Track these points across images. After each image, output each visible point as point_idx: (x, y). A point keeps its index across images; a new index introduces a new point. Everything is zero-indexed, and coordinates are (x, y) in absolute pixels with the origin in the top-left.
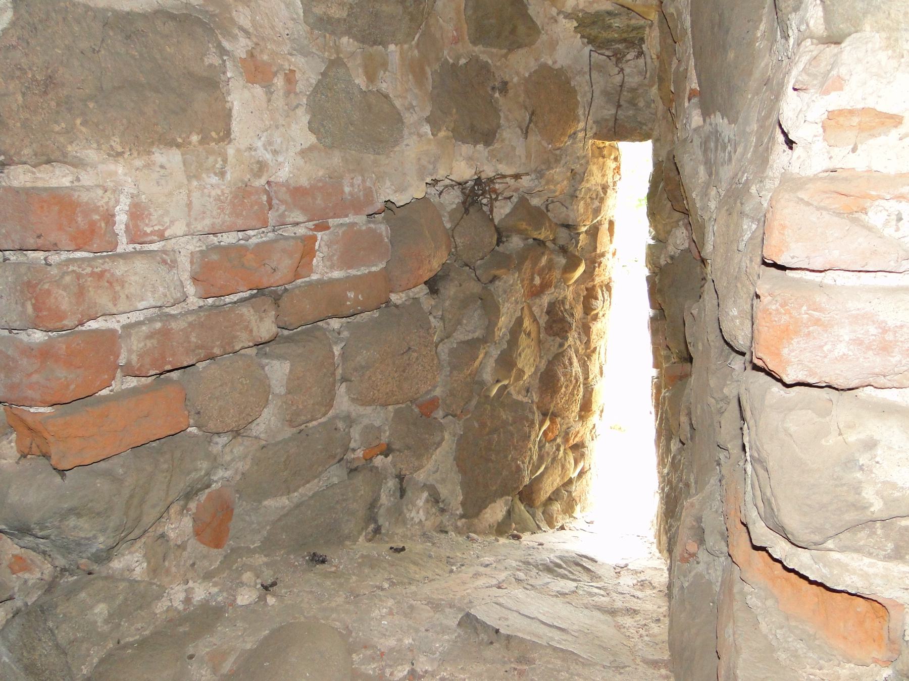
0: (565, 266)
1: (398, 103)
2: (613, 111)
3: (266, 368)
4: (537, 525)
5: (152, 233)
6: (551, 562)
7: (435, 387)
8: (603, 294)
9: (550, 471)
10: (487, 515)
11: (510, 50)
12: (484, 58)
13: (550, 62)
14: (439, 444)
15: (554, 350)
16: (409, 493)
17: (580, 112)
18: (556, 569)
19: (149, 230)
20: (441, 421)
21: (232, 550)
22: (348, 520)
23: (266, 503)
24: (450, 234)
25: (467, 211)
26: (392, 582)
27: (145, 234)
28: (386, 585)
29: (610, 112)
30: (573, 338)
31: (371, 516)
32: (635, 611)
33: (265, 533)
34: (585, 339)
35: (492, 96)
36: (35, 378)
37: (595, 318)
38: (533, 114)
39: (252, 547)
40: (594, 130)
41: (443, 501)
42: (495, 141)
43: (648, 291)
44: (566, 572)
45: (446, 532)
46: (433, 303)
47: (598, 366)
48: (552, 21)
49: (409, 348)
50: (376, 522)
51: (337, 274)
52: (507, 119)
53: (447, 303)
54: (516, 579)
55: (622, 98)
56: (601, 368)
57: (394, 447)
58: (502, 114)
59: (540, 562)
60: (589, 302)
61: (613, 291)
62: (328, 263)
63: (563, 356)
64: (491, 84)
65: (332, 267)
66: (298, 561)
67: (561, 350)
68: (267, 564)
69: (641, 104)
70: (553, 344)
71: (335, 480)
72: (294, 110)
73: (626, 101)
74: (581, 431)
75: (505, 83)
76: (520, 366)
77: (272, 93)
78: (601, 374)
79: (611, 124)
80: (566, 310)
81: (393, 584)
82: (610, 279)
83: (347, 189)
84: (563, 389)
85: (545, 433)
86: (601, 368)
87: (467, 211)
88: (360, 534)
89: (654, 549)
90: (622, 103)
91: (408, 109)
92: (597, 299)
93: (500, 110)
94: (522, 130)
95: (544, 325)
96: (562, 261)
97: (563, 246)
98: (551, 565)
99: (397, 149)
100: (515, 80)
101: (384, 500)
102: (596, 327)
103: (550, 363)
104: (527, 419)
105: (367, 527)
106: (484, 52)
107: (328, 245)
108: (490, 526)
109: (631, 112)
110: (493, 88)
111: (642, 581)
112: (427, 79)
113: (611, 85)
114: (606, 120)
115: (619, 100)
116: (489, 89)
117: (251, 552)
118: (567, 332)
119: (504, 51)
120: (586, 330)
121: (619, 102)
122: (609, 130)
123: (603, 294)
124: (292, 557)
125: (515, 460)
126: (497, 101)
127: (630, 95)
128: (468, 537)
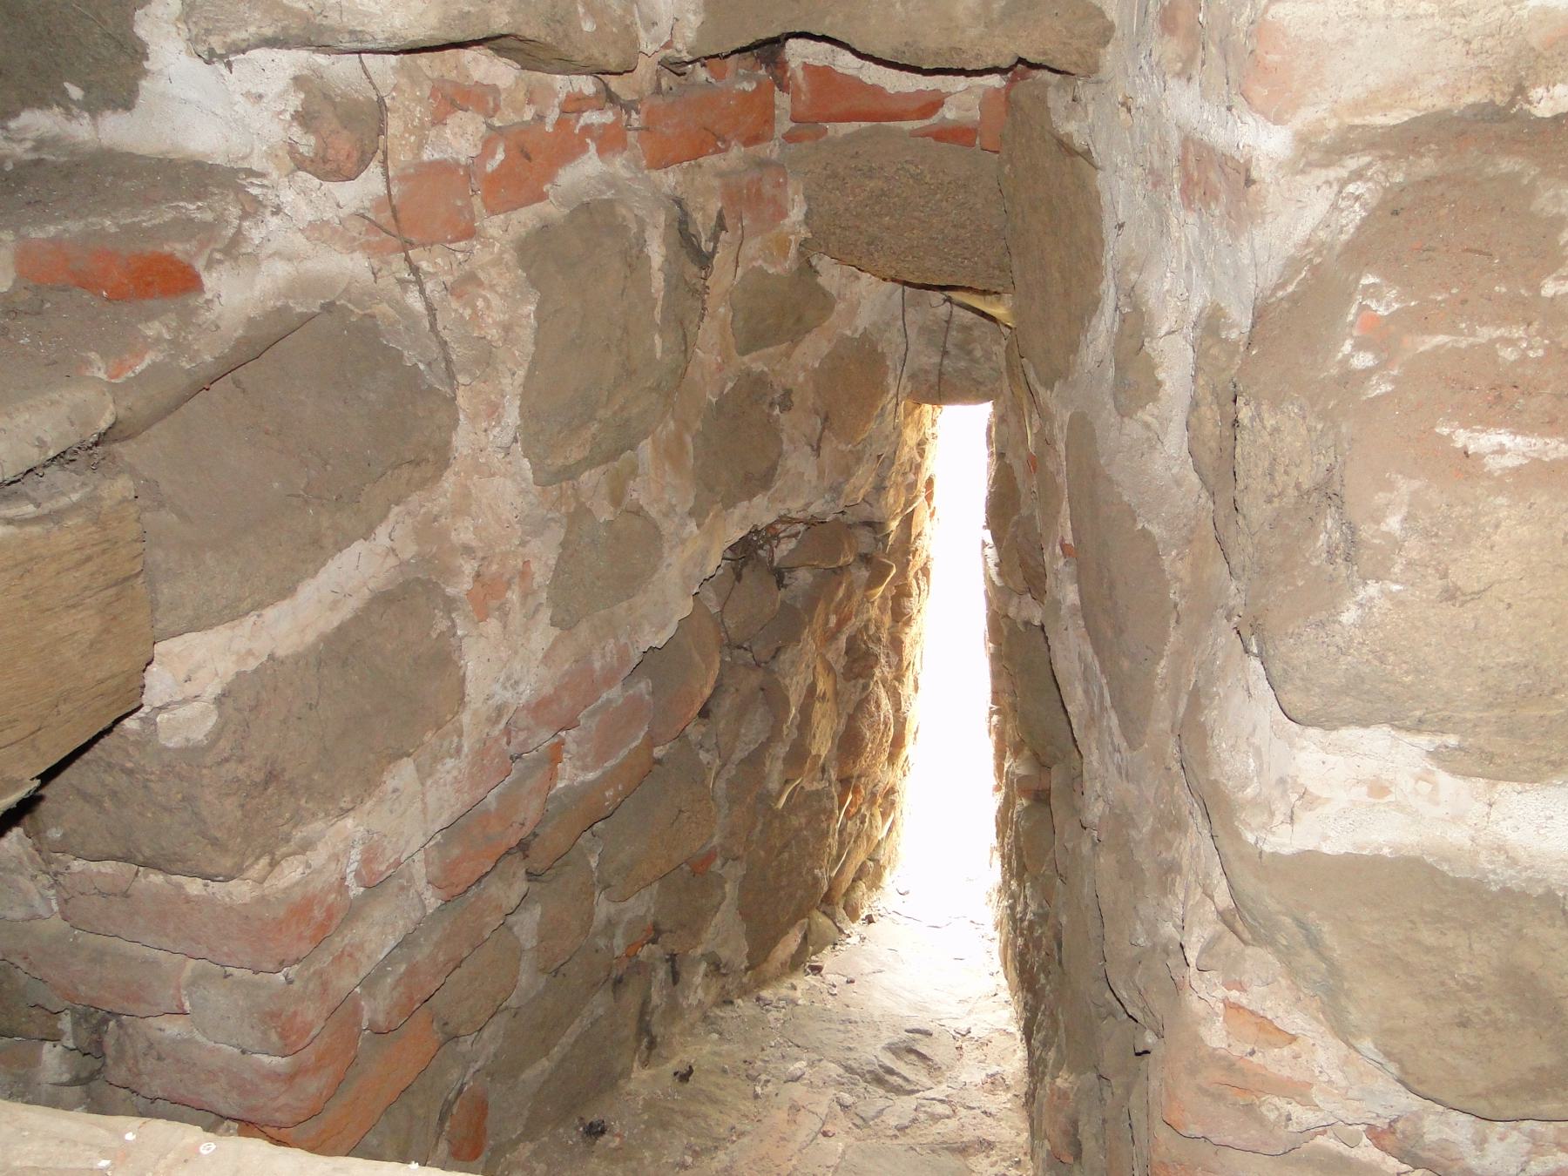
0: (868, 580)
1: (653, 512)
2: (936, 359)
3: (515, 929)
4: (838, 927)
5: (388, 868)
6: (880, 1066)
7: (711, 837)
8: (918, 584)
9: (853, 855)
10: (779, 952)
11: (795, 343)
12: (758, 367)
13: (848, 333)
14: (717, 908)
15: (856, 698)
16: (684, 975)
17: (890, 380)
18: (888, 1077)
19: (383, 868)
20: (720, 872)
21: (493, 1151)
22: (620, 1054)
23: (523, 1076)
24: (719, 620)
25: (739, 577)
26: (695, 1151)
27: (382, 873)
28: (689, 1160)
29: (932, 361)
30: (882, 671)
31: (644, 1029)
32: (989, 1143)
33: (526, 1113)
34: (894, 660)
35: (769, 415)
36: (282, 1100)
37: (908, 623)
38: (826, 419)
39: (514, 1137)
40: (908, 390)
41: (725, 966)
42: (776, 477)
43: (1004, 821)
44: (900, 1081)
45: (732, 1003)
46: (703, 729)
47: (911, 678)
48: (852, 278)
49: (680, 811)
50: (648, 1032)
51: (591, 776)
52: (792, 441)
53: (722, 725)
54: (841, 1105)
55: (950, 340)
56: (916, 681)
57: (662, 927)
58: (784, 437)
59: (867, 1068)
60: (899, 605)
61: (931, 576)
62: (579, 764)
63: (869, 702)
64: (769, 399)
65: (585, 769)
66: (571, 1139)
67: (864, 695)
68: (535, 1153)
69: (978, 353)
70: (853, 690)
71: (601, 1011)
72: (533, 617)
73: (956, 345)
74: (886, 776)
75: (788, 393)
76: (814, 752)
77: (507, 615)
78: (916, 689)
79: (933, 379)
80: (869, 637)
81: (696, 1154)
82: (928, 557)
83: (597, 665)
84: (870, 745)
85: (847, 811)
86: (916, 681)
87: (739, 577)
88: (632, 1061)
89: (997, 965)
90: (949, 347)
91: (666, 515)
92: (910, 595)
93: (782, 430)
94: (812, 447)
95: (842, 671)
96: (864, 574)
97: (866, 555)
98: (881, 1071)
99: (656, 576)
100: (801, 378)
101: (656, 999)
102: (909, 635)
103: (852, 718)
104: (824, 811)
105: (640, 1045)
106: (754, 360)
107: (576, 742)
108: (782, 964)
109: (962, 364)
110: (772, 405)
111: (992, 1075)
112: (687, 453)
113: (931, 318)
114: (926, 372)
115: (945, 343)
116: (765, 407)
117: (514, 1144)
118: (872, 667)
119: (784, 346)
120: (897, 645)
121: (944, 347)
122: (931, 387)
123: (918, 584)
124: (561, 1130)
125: (811, 870)
126: (778, 418)
127: (960, 336)
128: (758, 999)
